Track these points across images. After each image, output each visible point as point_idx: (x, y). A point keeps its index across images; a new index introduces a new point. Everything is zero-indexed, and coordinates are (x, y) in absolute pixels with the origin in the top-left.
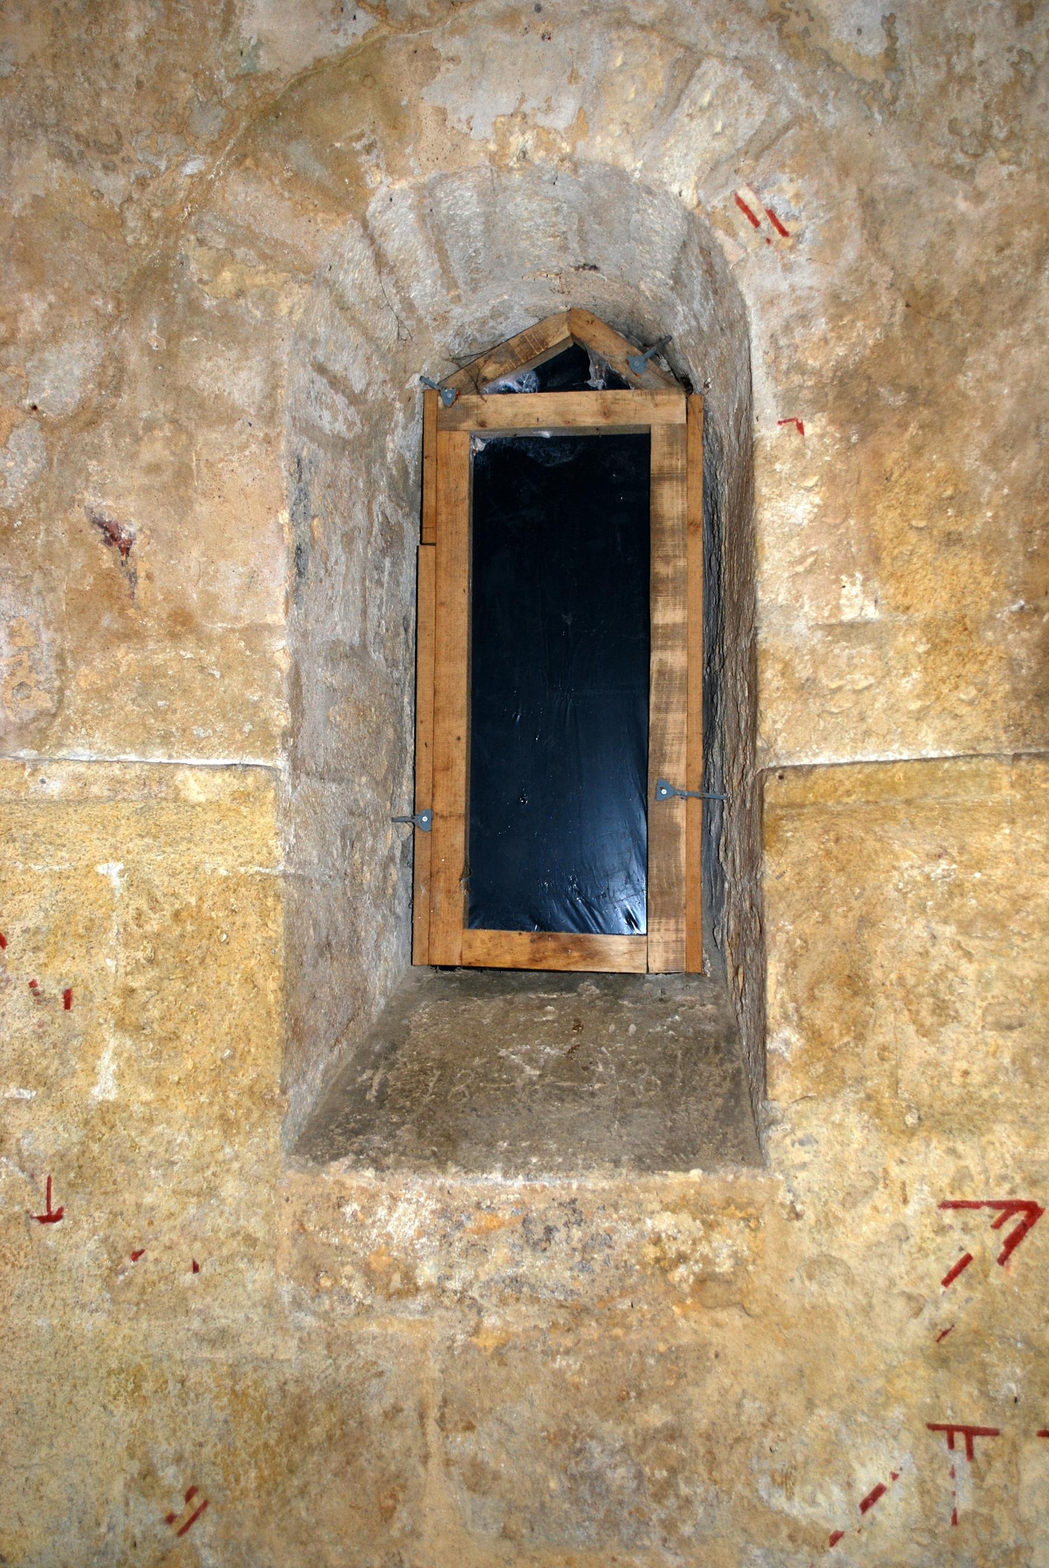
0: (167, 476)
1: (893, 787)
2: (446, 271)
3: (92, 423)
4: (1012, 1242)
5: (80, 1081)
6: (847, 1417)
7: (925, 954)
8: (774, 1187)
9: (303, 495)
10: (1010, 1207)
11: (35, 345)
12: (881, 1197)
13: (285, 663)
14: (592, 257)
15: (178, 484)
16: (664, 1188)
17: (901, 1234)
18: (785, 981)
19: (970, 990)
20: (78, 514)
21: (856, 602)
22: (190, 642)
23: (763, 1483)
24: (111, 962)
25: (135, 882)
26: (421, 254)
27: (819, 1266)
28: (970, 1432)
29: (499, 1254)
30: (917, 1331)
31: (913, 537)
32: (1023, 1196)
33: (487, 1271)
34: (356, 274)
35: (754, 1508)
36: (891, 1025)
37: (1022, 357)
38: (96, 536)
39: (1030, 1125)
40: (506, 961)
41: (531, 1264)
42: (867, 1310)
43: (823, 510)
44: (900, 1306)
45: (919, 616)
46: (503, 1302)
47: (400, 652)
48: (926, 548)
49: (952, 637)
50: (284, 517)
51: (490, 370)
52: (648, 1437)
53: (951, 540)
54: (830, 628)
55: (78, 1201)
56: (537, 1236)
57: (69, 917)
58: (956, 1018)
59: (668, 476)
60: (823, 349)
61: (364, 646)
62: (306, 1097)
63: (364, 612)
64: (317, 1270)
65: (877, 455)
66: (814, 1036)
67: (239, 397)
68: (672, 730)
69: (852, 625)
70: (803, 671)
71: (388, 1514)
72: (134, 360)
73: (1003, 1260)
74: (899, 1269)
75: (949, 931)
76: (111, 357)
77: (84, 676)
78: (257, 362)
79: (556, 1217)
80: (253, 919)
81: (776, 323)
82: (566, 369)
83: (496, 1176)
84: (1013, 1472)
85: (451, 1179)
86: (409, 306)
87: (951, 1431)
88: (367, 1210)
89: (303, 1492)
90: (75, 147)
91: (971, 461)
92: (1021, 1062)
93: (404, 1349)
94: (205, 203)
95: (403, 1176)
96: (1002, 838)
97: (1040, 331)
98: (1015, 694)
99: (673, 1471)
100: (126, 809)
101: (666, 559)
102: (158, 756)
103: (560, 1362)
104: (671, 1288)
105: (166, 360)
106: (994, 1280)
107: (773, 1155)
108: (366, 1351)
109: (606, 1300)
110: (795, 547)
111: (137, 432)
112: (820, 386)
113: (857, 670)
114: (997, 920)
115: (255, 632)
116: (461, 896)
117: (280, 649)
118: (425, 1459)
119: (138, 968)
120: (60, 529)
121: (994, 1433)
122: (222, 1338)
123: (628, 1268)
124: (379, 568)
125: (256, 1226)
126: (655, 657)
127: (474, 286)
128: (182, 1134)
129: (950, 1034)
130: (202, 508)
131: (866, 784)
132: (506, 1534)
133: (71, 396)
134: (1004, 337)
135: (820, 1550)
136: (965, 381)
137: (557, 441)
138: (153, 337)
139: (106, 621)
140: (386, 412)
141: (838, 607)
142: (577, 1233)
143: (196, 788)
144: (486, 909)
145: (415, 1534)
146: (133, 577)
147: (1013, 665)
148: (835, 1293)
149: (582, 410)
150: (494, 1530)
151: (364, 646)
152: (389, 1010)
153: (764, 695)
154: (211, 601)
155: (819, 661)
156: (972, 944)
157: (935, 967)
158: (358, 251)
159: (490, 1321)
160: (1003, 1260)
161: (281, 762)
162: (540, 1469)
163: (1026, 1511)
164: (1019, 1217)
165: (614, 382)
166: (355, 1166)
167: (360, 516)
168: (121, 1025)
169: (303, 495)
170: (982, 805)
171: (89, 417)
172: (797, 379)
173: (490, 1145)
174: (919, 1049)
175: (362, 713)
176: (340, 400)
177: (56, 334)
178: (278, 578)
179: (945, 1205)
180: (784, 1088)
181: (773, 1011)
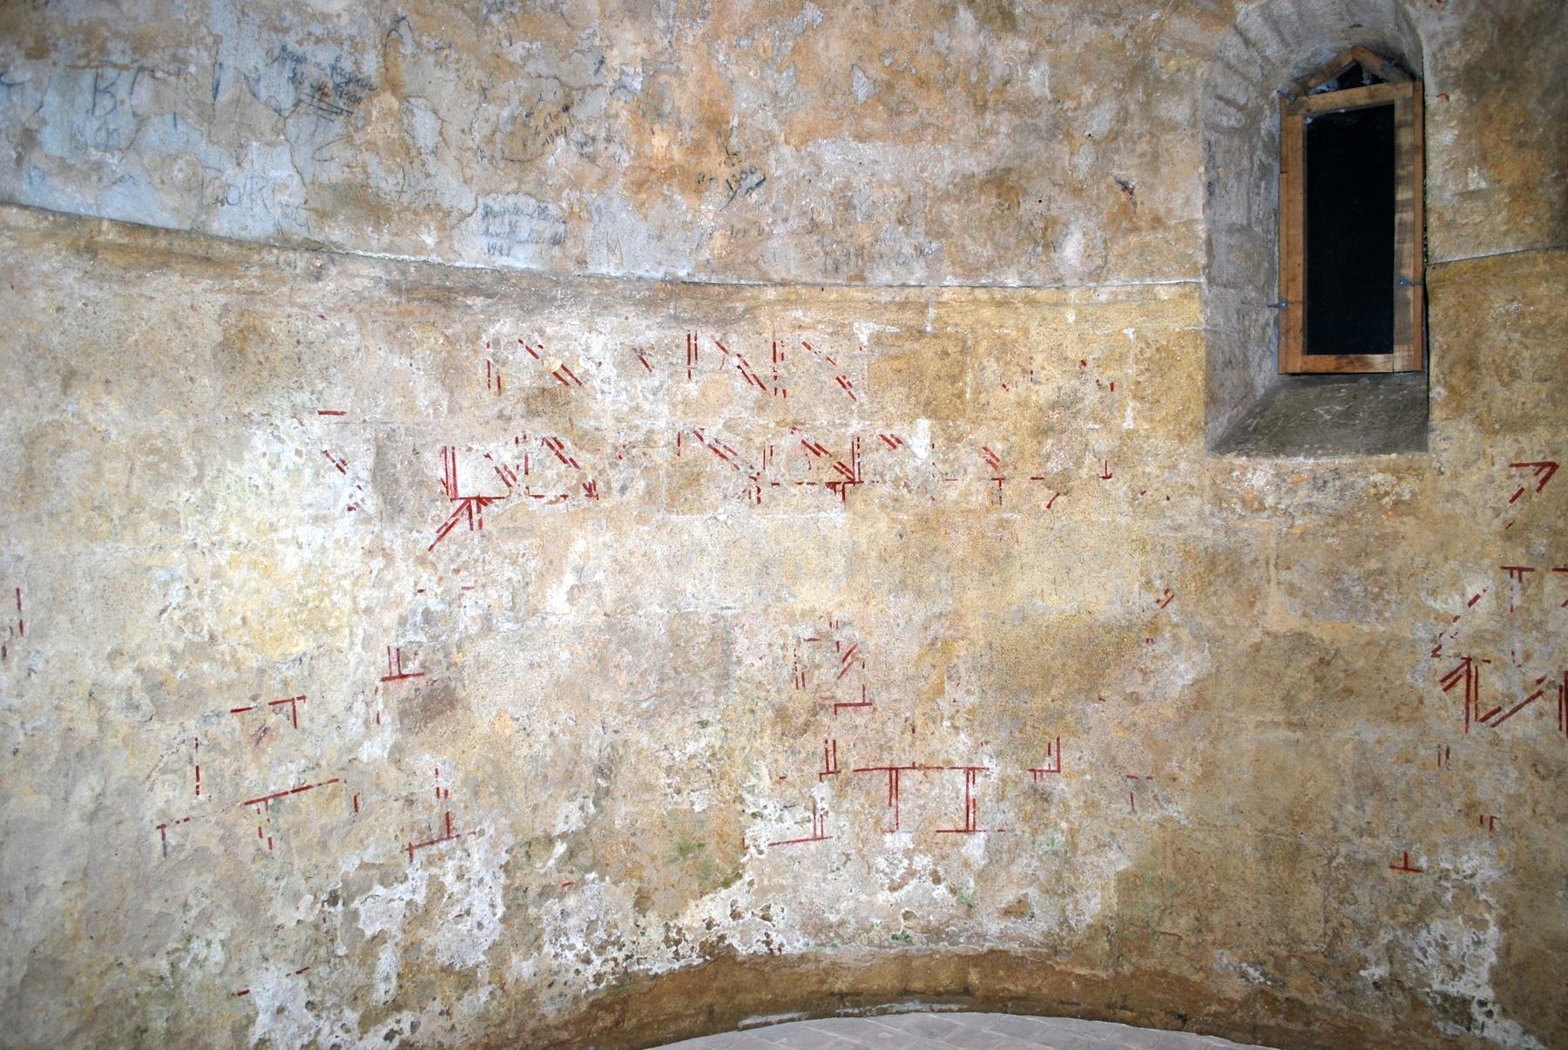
0: (1148, 158)
1: (1486, 268)
2: (1283, 39)
3: (1115, 139)
4: (1544, 482)
5: (1118, 421)
6: (1463, 564)
7: (1505, 348)
8: (1432, 460)
9: (1212, 158)
10: (1543, 465)
11: (1089, 108)
12: (1481, 464)
13: (1203, 236)
14: (1357, 20)
15: (1153, 161)
16: (1379, 462)
17: (1491, 480)
18: (1439, 364)
19: (1526, 363)
20: (1111, 179)
21: (1476, 180)
22: (1161, 230)
23: (1423, 594)
24: (1131, 371)
25: (1140, 336)
26: (1268, 35)
27: (1452, 496)
28: (1521, 570)
29: (1302, 493)
30: (1497, 524)
31: (1503, 145)
32: (1549, 460)
33: (1296, 501)
34: (1234, 49)
35: (1418, 605)
36: (1489, 382)
37: (1556, 49)
38: (1120, 187)
39: (1553, 426)
40: (1323, 370)
41: (1317, 497)
42: (1474, 515)
43: (1458, 137)
44: (1489, 513)
45: (1506, 184)
46: (1304, 514)
47: (1272, 226)
48: (1510, 150)
49: (1522, 193)
50: (1202, 169)
51: (1312, 83)
52: (1370, 574)
53: (1522, 145)
54: (1462, 194)
55: (1119, 470)
56: (1319, 484)
57: (1112, 352)
58: (1520, 377)
59: (1404, 125)
60: (1458, 57)
61: (1249, 225)
62: (1220, 426)
63: (1249, 208)
64: (1221, 500)
65: (1486, 106)
66: (1452, 390)
67: (1179, 118)
68: (1406, 252)
69: (1473, 192)
70: (1448, 217)
71: (1252, 604)
72: (1132, 108)
73: (1539, 490)
74: (1490, 495)
75: (1517, 336)
76: (1122, 108)
77: (1117, 249)
78: (1187, 101)
79: (1329, 476)
80: (1191, 350)
81: (1436, 47)
82: (1350, 77)
83: (1301, 459)
84: (1540, 587)
85: (1281, 461)
86: (1266, 59)
87: (1511, 569)
88: (1243, 474)
89: (1215, 593)
90: (1101, 18)
91: (1532, 105)
92: (1551, 397)
93: (1259, 534)
94: (1161, 31)
95: (1260, 459)
96: (1542, 289)
97: (1564, 35)
98: (1552, 218)
99: (1382, 589)
100: (1134, 305)
101: (1403, 167)
102: (1148, 281)
103: (1330, 540)
104: (1381, 507)
105: (1146, 106)
106: (1534, 499)
107: (1431, 445)
108: (1242, 535)
109: (1351, 513)
110: (1445, 158)
111: (1133, 140)
112: (1457, 76)
113: (1474, 214)
114: (1541, 329)
115: (1190, 223)
116: (1300, 340)
117: (1201, 229)
118: (1269, 581)
119: (1142, 373)
120: (1103, 186)
121: (1532, 570)
122: (1178, 528)
123: (1362, 499)
124: (1258, 187)
125: (1194, 481)
126: (1397, 217)
127: (1300, 44)
128: (1162, 442)
129: (1517, 385)
130: (1165, 170)
131: (1475, 267)
132: (1305, 615)
133: (1105, 128)
134: (1547, 39)
135: (1449, 624)
136: (1529, 64)
137: (1349, 113)
138: (1140, 95)
139: (1124, 225)
140: (1260, 110)
141: (1467, 184)
142: (1338, 483)
143: (1163, 295)
144: (1314, 345)
145: (1264, 613)
146: (1135, 204)
147: (1552, 204)
148: (1459, 507)
149: (1359, 96)
150: (1299, 613)
151: (1249, 225)
152: (1266, 394)
153: (1430, 230)
154: (1169, 212)
155: (1456, 211)
156: (1528, 342)
157: (1510, 354)
158: (1235, 40)
159: (1298, 522)
160: (1539, 490)
161: (1203, 280)
162: (1320, 587)
163: (1546, 605)
164: (1547, 470)
165: (1376, 80)
166: (1238, 455)
167: (1246, 163)
168: (1135, 397)
169: (1212, 158)
170: (1530, 274)
171: (1113, 136)
172: (1446, 73)
173: (1301, 446)
174: (1501, 393)
175: (1248, 256)
176: (1232, 110)
177: (1097, 102)
178: (1199, 197)
179: (1512, 465)
180: (1437, 415)
181: (1433, 379)
